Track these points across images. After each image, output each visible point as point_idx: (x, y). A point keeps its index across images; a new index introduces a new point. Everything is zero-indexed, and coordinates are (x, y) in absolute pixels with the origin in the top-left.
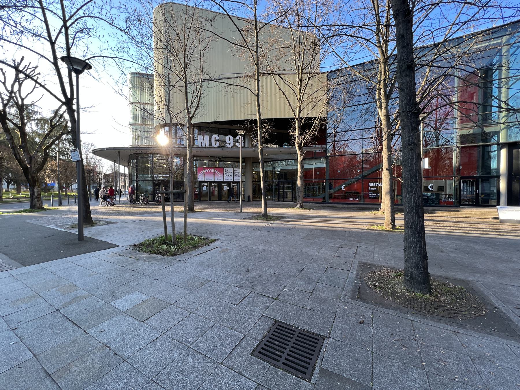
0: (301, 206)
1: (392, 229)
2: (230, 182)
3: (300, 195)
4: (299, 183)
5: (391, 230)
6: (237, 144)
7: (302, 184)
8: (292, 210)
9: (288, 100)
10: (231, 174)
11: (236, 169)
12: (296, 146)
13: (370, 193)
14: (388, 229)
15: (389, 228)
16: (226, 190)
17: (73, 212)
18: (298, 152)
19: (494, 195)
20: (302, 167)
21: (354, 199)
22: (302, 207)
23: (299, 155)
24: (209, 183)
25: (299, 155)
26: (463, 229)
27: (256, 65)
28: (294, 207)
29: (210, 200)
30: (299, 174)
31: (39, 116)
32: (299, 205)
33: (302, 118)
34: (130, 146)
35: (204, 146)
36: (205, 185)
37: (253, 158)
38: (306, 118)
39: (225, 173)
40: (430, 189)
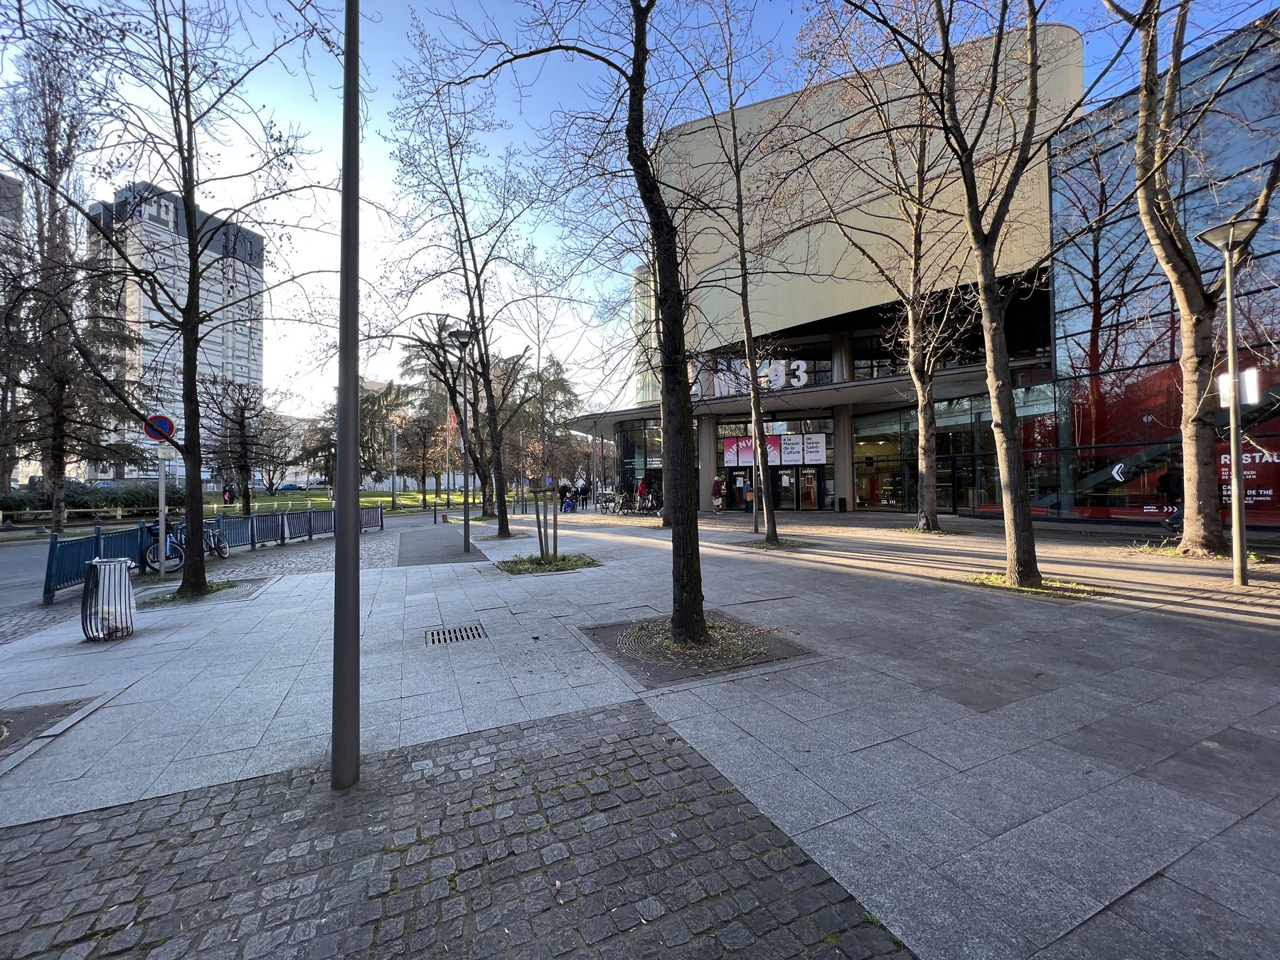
0: (927, 524)
1: (1020, 585)
2: (797, 466)
3: (927, 495)
4: (922, 465)
5: (1016, 586)
6: (794, 382)
7: (928, 467)
8: (908, 535)
9: (876, 264)
10: (799, 448)
11: (809, 436)
12: (911, 368)
13: (477, 501)
14: (1008, 584)
15: (1009, 580)
16: (787, 485)
17: (712, 537)
18: (918, 384)
19: (155, 502)
20: (930, 423)
21: (1160, 508)
22: (932, 527)
23: (920, 393)
24: (797, 469)
25: (920, 393)
26: (1117, 592)
27: (481, 374)
28: (911, 525)
29: (798, 509)
30: (922, 441)
31: (527, 372)
32: (922, 522)
33: (923, 297)
34: (635, 407)
35: (725, 394)
36: (787, 475)
37: (855, 405)
38: (932, 294)
39: (783, 446)
40: (1117, 478)
